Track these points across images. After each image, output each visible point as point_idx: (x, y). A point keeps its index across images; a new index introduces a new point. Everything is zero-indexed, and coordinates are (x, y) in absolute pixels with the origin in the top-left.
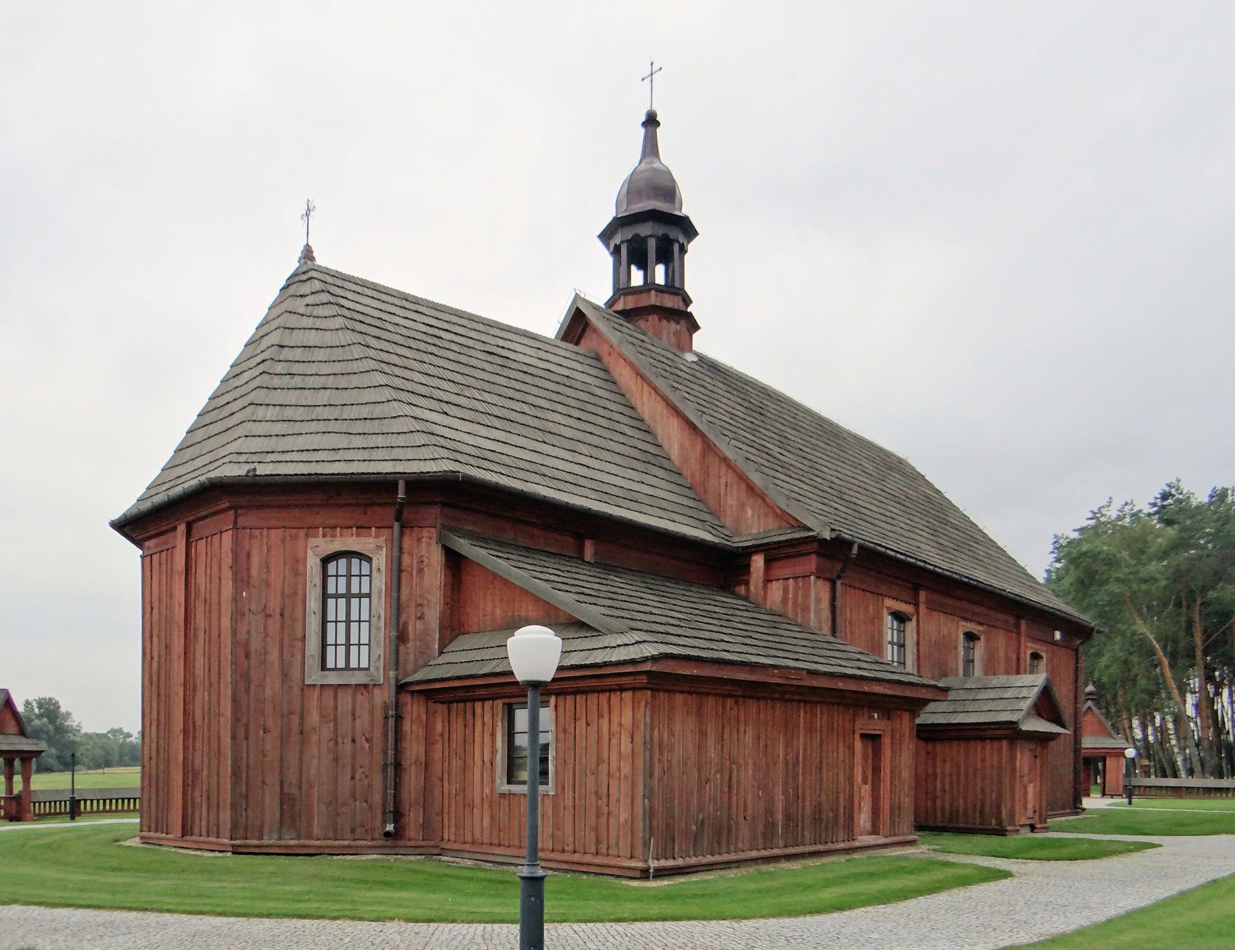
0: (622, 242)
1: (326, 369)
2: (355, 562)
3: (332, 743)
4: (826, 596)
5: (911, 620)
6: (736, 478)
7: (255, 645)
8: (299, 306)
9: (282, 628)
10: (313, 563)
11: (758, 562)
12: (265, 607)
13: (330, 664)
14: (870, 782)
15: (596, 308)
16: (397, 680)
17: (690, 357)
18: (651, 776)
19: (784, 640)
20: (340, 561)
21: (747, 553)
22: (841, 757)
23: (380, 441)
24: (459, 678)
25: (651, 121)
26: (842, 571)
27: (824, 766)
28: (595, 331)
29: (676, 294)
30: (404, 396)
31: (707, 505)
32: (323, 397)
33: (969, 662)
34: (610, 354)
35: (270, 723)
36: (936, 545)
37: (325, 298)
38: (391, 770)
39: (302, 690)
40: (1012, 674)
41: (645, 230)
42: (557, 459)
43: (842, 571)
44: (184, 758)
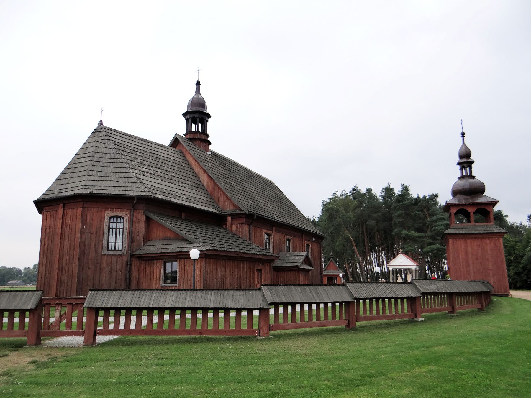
0: (189, 118)
1: (110, 161)
2: (119, 219)
3: (110, 272)
4: (248, 229)
5: (271, 235)
6: (223, 194)
7: (87, 242)
8: (100, 139)
9: (96, 237)
10: (106, 218)
11: (229, 219)
12: (91, 232)
13: (110, 248)
14: (259, 283)
15: (181, 137)
16: (131, 254)
17: (209, 153)
18: (205, 280)
19: (237, 243)
20: (114, 218)
21: (226, 216)
22: (251, 276)
23: (128, 185)
24: (151, 254)
25: (198, 84)
26: (252, 222)
27: (247, 278)
28: (181, 144)
29: (205, 135)
30: (133, 170)
31: (215, 201)
32: (110, 170)
33: (288, 247)
34: (186, 152)
35: (90, 266)
36: (278, 212)
37: (107, 138)
38: (128, 281)
39: (101, 256)
40: (301, 252)
41: (196, 115)
42: (175, 189)
43: (252, 222)
44: (57, 277)
